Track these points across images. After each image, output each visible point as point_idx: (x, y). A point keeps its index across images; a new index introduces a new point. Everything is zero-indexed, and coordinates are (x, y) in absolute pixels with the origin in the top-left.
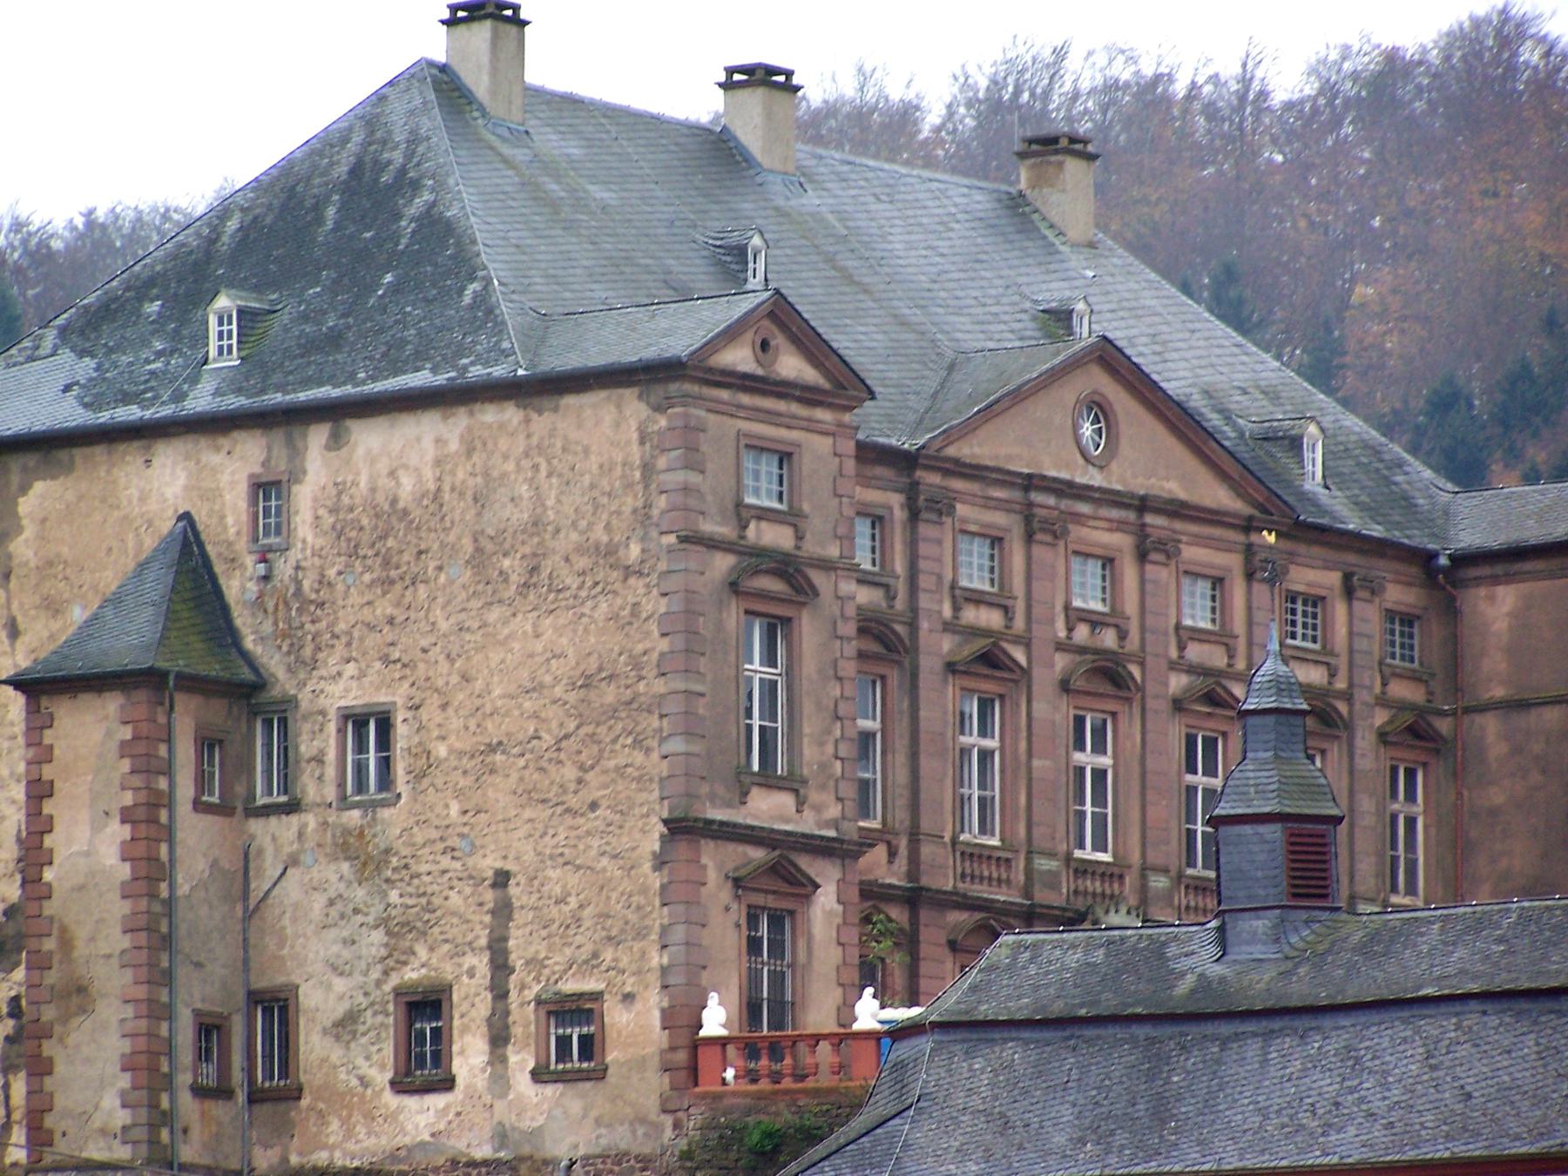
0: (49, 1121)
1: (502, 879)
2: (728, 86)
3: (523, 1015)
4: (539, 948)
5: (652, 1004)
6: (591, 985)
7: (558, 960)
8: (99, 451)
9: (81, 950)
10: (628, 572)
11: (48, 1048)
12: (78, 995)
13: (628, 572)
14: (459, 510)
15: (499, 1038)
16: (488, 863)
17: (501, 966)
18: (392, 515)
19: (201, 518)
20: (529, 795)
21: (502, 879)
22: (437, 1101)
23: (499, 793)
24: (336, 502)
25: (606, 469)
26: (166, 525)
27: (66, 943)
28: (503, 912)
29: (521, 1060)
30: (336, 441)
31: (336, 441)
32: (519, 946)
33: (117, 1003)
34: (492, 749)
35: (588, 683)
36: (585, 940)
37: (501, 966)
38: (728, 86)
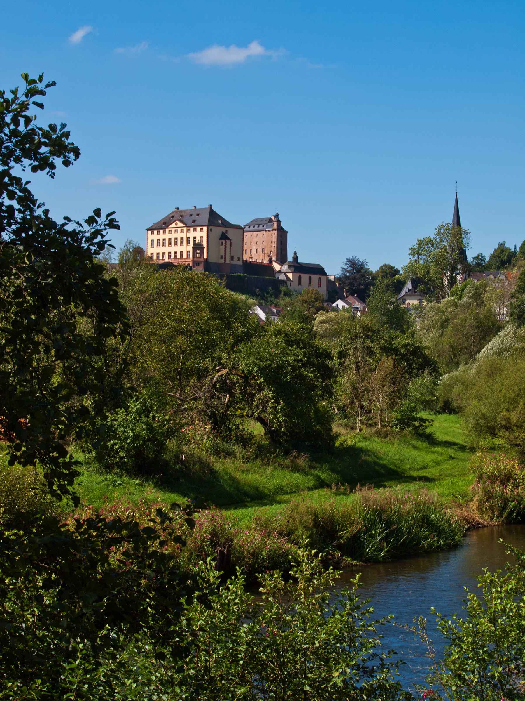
33: (256, 258)
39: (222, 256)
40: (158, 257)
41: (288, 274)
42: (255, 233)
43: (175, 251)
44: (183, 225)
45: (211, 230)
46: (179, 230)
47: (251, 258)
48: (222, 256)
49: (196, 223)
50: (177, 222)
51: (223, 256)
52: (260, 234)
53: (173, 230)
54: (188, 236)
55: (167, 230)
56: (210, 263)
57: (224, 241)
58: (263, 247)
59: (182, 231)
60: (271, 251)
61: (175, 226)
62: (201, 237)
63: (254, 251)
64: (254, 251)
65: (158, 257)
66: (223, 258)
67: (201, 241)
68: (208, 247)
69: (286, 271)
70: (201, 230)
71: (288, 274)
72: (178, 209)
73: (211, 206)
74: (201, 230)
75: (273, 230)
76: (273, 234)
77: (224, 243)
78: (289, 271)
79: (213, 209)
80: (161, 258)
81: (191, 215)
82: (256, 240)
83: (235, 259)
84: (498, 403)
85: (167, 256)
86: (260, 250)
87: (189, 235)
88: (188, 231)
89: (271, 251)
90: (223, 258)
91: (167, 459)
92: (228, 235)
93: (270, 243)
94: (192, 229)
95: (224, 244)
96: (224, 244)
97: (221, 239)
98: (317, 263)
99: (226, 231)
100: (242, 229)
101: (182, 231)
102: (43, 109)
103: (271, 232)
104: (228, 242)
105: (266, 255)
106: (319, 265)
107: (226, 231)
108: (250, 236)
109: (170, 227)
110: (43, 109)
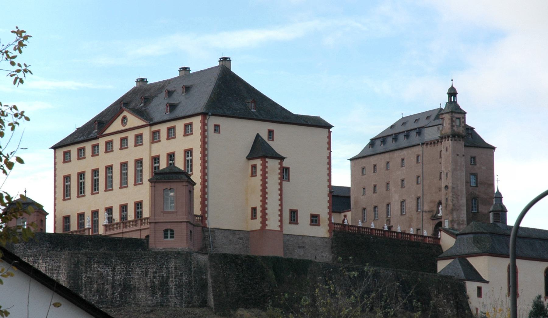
39: (254, 210)
40: (81, 224)
41: (471, 260)
43: (66, 174)
45: (217, 128)
48: (254, 210)
49: (179, 112)
50: (125, 113)
51: (259, 209)
52: (409, 155)
53: (116, 139)
54: (154, 154)
55: (102, 142)
56: (214, 230)
57: (258, 162)
58: (420, 194)
59: (139, 139)
61: (123, 128)
62: (188, 152)
63: (395, 208)
64: (395, 208)
65: (81, 224)
66: (259, 214)
67: (189, 163)
68: (204, 181)
69: (466, 251)
70: (188, 130)
71: (471, 260)
74: (188, 130)
75: (443, 138)
77: (259, 168)
78: (476, 250)
80: (88, 224)
82: (398, 174)
83: (304, 218)
84: (205, 238)
86: (411, 204)
88: (155, 137)
90: (259, 214)
92: (276, 145)
95: (259, 172)
96: (259, 172)
97: (250, 157)
99: (271, 133)
101: (139, 139)
103: (439, 147)
104: (273, 165)
105: (427, 216)
107: (271, 133)
108: (383, 165)
109: (108, 131)
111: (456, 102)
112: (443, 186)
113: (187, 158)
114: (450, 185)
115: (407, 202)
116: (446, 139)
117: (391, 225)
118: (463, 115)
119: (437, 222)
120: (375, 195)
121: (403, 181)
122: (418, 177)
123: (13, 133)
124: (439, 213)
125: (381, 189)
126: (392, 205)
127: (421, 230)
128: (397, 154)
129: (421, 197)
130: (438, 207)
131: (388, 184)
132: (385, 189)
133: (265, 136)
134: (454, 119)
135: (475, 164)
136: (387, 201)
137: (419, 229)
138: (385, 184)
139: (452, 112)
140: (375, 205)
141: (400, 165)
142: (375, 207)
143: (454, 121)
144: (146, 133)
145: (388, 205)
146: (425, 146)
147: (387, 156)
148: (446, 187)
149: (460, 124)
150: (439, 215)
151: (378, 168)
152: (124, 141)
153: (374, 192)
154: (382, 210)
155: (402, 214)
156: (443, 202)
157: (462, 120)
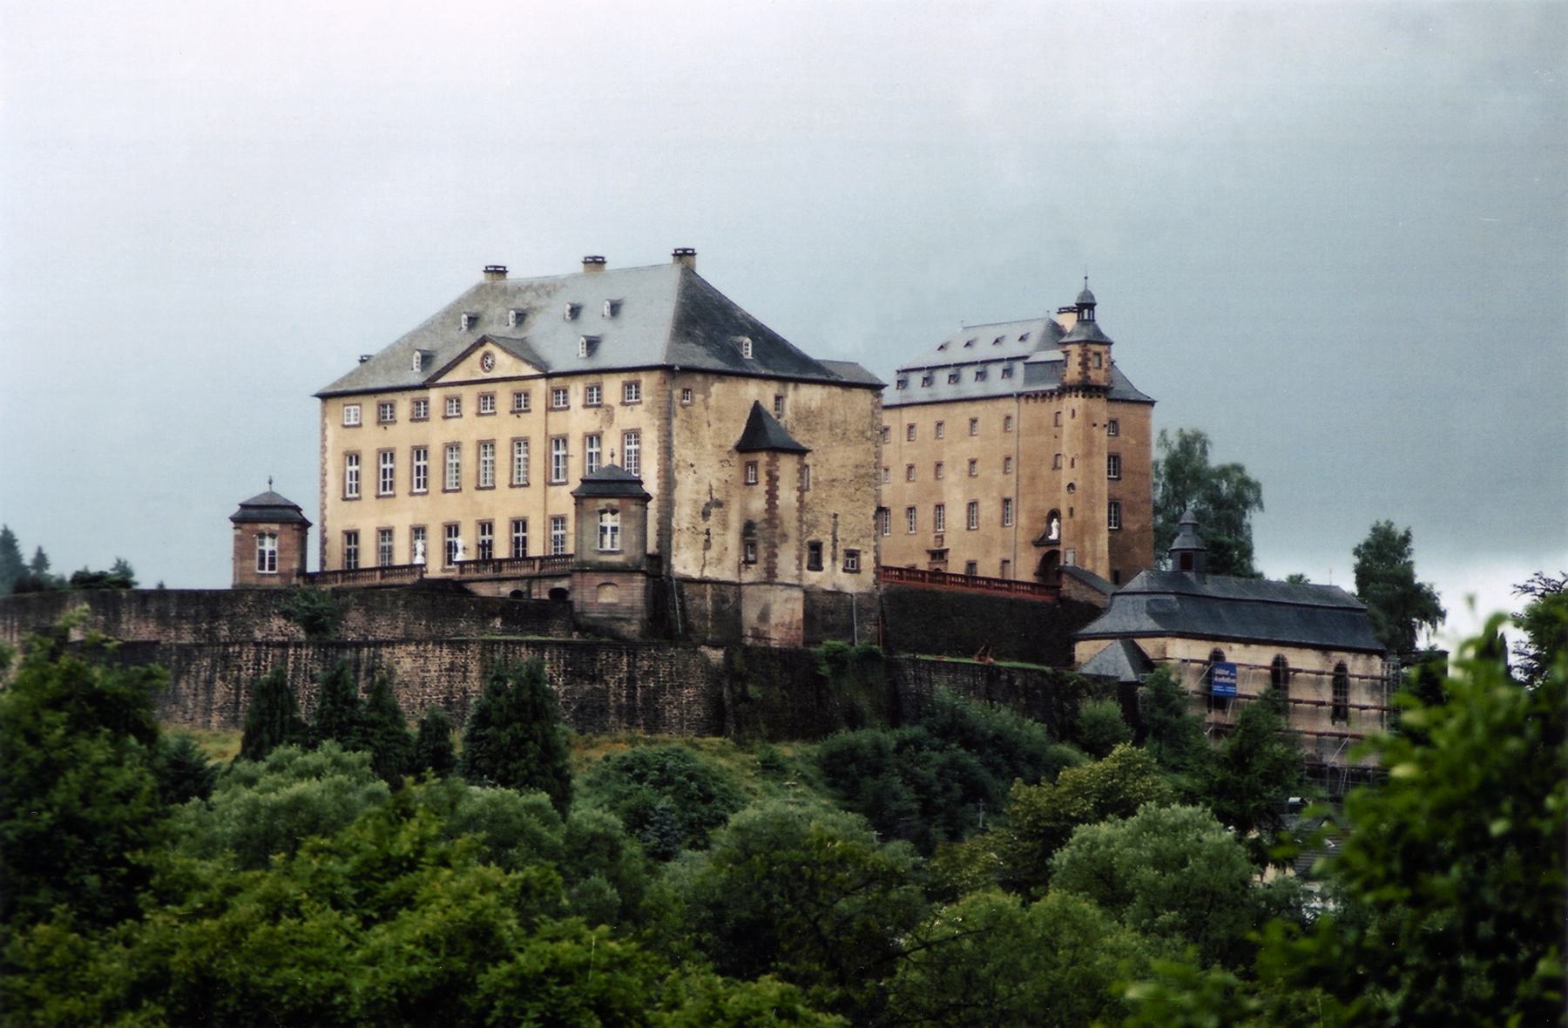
0: (326, 535)
1: (835, 516)
2: (585, 263)
3: (840, 553)
4: (844, 536)
5: (871, 555)
6: (857, 548)
7: (849, 540)
8: (734, 379)
9: (786, 524)
10: (868, 439)
11: (776, 551)
12: (784, 537)
13: (868, 439)
14: (826, 414)
15: (834, 559)
16: (832, 511)
17: (835, 540)
18: (810, 413)
19: (761, 403)
20: (843, 495)
21: (835, 516)
22: (818, 573)
23: (836, 492)
24: (796, 406)
25: (862, 410)
26: (752, 403)
27: (782, 523)
28: (836, 524)
29: (840, 566)
30: (796, 388)
31: (796, 388)
32: (840, 535)
33: (970, 556)
34: (833, 480)
35: (857, 466)
36: (856, 535)
37: (835, 540)
38: (585, 263)
42: (961, 414)
44: (528, 370)
46: (504, 395)
47: (939, 555)
53: (469, 396)
54: (554, 431)
59: (521, 405)
60: (1054, 514)
63: (956, 516)
64: (956, 516)
71: (1142, 643)
72: (498, 272)
73: (684, 255)
76: (1066, 418)
79: (705, 269)
81: (615, 308)
82: (970, 447)
85: (435, 539)
86: (989, 509)
87: (559, 424)
89: (1054, 514)
91: (238, 829)
93: (1046, 471)
94: (577, 390)
98: (1327, 583)
100: (876, 388)
101: (521, 405)
102: (5, 526)
103: (1053, 406)
104: (787, 465)
106: (1337, 587)
108: (931, 427)
110: (5, 526)
111: (1093, 320)
112: (1065, 483)
113: (627, 447)
114: (1078, 484)
115: (980, 505)
116: (1073, 394)
117: (945, 547)
118: (1106, 347)
119: (1045, 550)
120: (910, 485)
121: (973, 462)
122: (1008, 459)
123: (545, 509)
124: (1050, 533)
125: (925, 474)
126: (947, 509)
127: (1012, 563)
128: (959, 409)
129: (1014, 500)
130: (1049, 521)
131: (939, 465)
132: (933, 476)
133: (768, 404)
134: (1090, 355)
135: (1117, 435)
136: (937, 501)
137: (1008, 562)
138: (932, 467)
139: (1086, 342)
140: (909, 503)
141: (967, 431)
142: (911, 509)
143: (1089, 359)
144: (540, 388)
145: (940, 507)
146: (1022, 400)
147: (938, 413)
148: (1071, 486)
149: (1100, 365)
150: (1051, 537)
151: (918, 432)
152: (487, 400)
153: (908, 479)
154: (925, 515)
155: (969, 529)
156: (1064, 513)
157: (1104, 357)
